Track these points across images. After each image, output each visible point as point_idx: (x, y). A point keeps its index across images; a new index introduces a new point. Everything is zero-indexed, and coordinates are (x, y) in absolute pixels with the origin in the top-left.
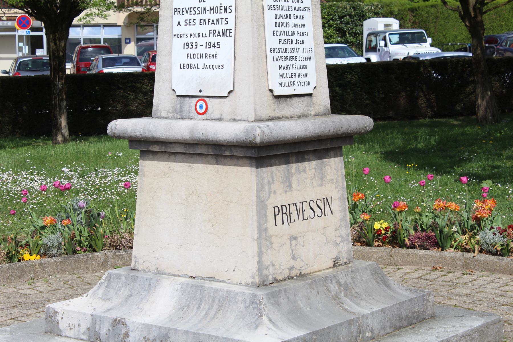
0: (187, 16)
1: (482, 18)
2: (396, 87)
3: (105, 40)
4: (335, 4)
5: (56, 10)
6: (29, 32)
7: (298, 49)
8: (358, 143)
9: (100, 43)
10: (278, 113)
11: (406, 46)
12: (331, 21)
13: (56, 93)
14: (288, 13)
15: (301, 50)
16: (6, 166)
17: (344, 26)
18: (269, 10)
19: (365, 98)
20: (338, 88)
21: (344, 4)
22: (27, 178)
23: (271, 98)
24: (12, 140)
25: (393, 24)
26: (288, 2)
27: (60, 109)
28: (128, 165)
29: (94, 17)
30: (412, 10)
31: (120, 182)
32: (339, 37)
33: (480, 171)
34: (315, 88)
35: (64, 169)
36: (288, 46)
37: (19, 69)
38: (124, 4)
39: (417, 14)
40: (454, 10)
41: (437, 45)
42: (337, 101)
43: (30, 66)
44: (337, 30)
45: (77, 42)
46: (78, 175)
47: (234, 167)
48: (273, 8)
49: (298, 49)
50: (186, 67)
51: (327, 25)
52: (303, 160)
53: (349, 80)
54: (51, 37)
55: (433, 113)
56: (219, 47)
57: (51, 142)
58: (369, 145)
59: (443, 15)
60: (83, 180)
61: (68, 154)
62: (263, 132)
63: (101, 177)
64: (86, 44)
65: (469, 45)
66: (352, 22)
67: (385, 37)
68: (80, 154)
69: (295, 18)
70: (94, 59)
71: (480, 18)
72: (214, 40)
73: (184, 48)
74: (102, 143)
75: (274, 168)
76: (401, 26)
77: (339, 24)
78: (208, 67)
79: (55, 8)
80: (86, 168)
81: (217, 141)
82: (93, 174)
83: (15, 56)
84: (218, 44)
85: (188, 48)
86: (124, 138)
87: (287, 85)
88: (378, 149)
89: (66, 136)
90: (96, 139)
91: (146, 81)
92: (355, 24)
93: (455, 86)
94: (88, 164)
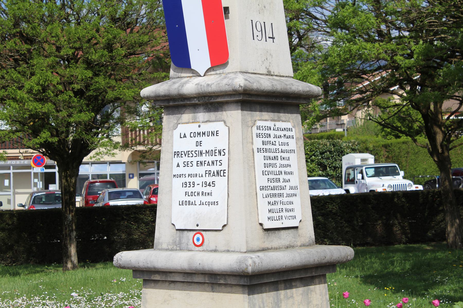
0: (186, 159)
1: (448, 153)
2: (373, 216)
3: (111, 176)
4: (317, 142)
5: (68, 150)
6: (43, 169)
7: (285, 187)
8: (339, 268)
9: (107, 178)
10: (267, 245)
11: (381, 178)
12: (313, 157)
13: (67, 224)
14: (275, 154)
15: (288, 188)
16: (20, 292)
17: (324, 161)
18: (258, 152)
19: (345, 226)
20: (320, 217)
21: (324, 142)
22: (39, 303)
23: (261, 231)
24: (26, 268)
25: (369, 159)
26: (275, 145)
27: (70, 239)
28: (131, 289)
29: (103, 156)
30: (386, 146)
31: (124, 306)
32: (320, 170)
33: (452, 294)
34: (301, 221)
35: (73, 294)
36: (276, 184)
37: (34, 203)
38: (128, 144)
39: (391, 150)
40: (424, 147)
41: (409, 177)
42: (320, 229)
43: (44, 200)
44: (318, 165)
45: (86, 178)
46: (86, 299)
47: (228, 294)
48: (262, 151)
49: (285, 187)
50: (184, 204)
51: (309, 160)
52: (291, 287)
53: (330, 209)
54: (63, 174)
55: (407, 239)
56: (214, 186)
57: (61, 269)
58: (350, 270)
59: (414, 150)
60: (90, 304)
61: (77, 280)
62: (254, 262)
63: (106, 301)
64: (94, 179)
65: (438, 177)
66: (332, 157)
67: (362, 170)
68: (88, 280)
69: (282, 159)
70: (101, 192)
71: (447, 154)
72: (209, 179)
73: (183, 187)
74: (108, 269)
75: (264, 295)
76: (376, 161)
77: (320, 159)
78: (204, 204)
79: (67, 149)
80: (93, 292)
81: (212, 271)
82: (99, 298)
83: (30, 191)
84: (213, 183)
85: (186, 187)
86: (128, 268)
87: (276, 219)
88: (358, 273)
89: (75, 263)
90: (102, 266)
91: (148, 212)
92: (335, 159)
93: (426, 214)
94: (94, 289)
